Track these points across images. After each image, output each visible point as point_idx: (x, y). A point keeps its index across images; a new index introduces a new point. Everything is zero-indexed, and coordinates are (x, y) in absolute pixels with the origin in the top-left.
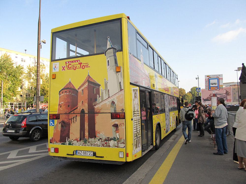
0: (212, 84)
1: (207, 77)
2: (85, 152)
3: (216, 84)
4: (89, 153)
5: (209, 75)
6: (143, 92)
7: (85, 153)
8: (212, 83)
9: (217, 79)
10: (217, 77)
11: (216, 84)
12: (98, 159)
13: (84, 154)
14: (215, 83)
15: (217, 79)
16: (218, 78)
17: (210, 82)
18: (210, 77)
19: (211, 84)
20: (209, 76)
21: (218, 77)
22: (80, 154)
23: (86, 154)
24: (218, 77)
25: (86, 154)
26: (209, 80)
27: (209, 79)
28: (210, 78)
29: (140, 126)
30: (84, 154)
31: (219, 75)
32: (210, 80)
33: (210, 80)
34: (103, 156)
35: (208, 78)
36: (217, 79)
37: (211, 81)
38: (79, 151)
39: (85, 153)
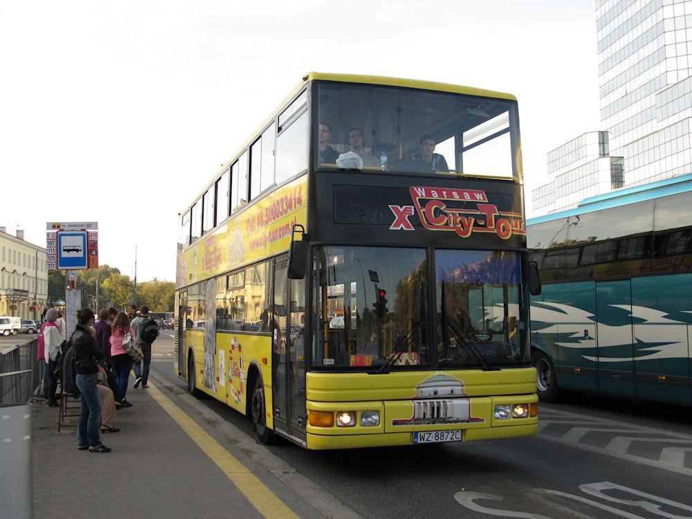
0: (68, 251)
1: (54, 227)
2: (440, 433)
3: (77, 251)
4: (450, 435)
5: (60, 223)
6: (443, 341)
7: (440, 436)
8: (68, 248)
9: (84, 235)
10: (82, 230)
11: (77, 251)
12: (489, 135)
13: (437, 438)
14: (76, 248)
15: (82, 237)
16: (86, 233)
17: (63, 245)
18: (61, 228)
19: (64, 250)
20: (59, 227)
21: (84, 230)
22: (425, 439)
23: (442, 438)
24: (84, 230)
25: (442, 438)
26: (58, 238)
27: (58, 232)
28: (63, 230)
29: (422, 196)
30: (437, 438)
31: (89, 225)
32: (62, 237)
33: (62, 237)
34: (1, 248)
35: (57, 233)
36: (82, 237)
37: (67, 242)
38: (422, 434)
39: (440, 436)
